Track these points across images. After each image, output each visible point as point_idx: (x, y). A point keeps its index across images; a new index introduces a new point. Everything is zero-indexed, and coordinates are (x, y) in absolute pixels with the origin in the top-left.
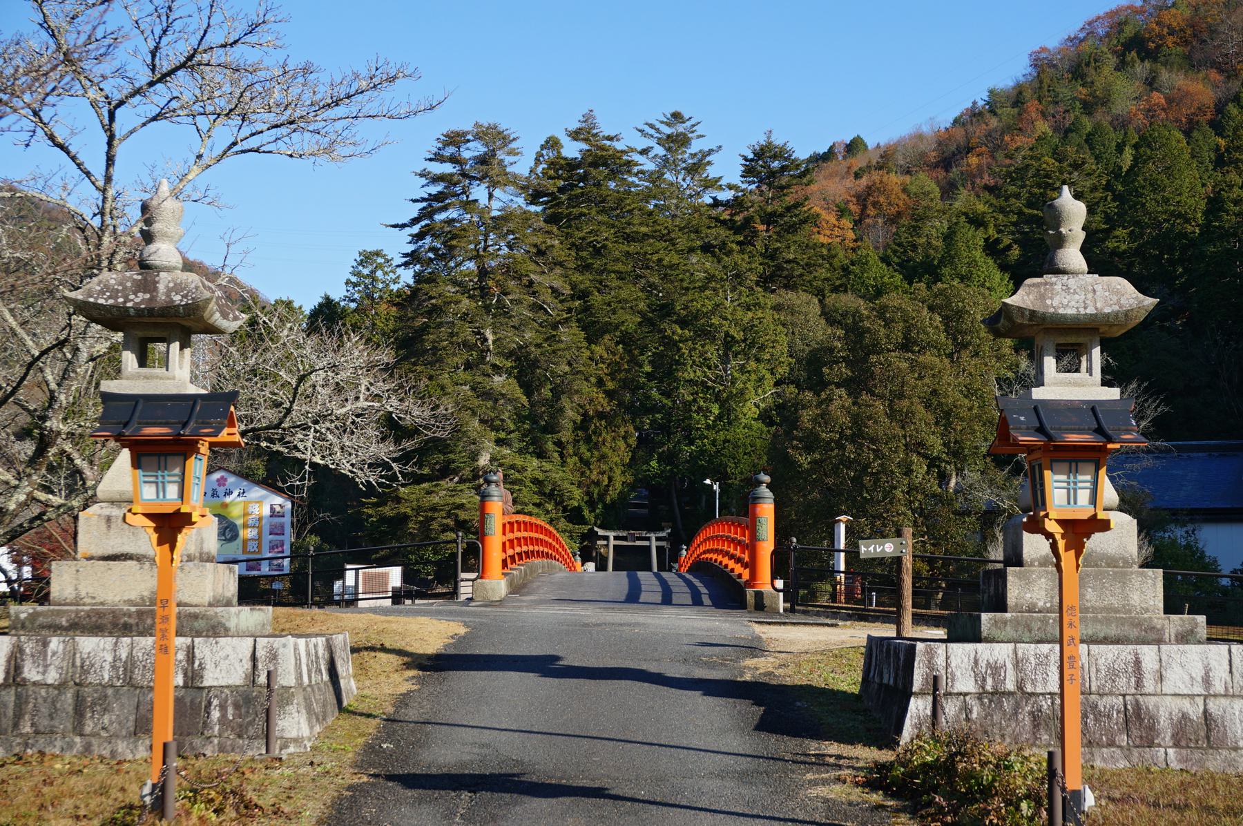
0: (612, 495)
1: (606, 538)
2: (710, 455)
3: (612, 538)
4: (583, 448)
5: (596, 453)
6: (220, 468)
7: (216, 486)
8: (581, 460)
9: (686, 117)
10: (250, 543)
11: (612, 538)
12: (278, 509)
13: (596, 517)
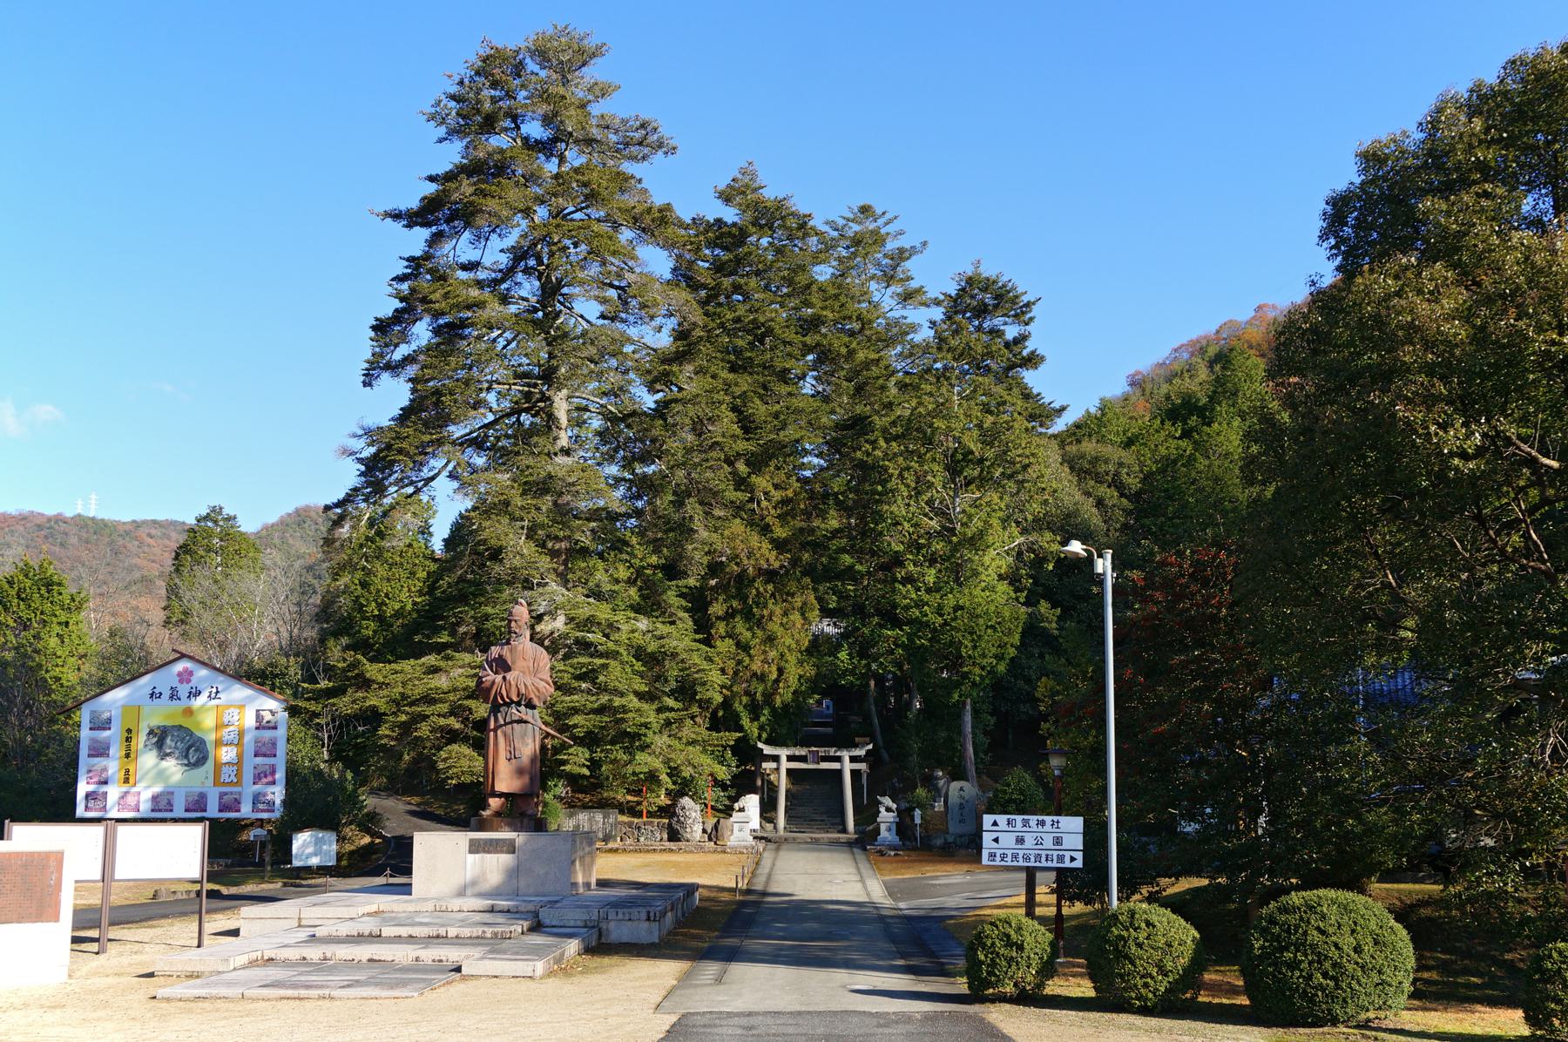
0: (784, 696)
1: (776, 759)
2: (935, 630)
3: (784, 759)
4: (740, 626)
5: (759, 633)
6: (183, 656)
7: (175, 683)
8: (738, 645)
9: (879, 211)
10: (225, 769)
11: (784, 759)
12: (267, 716)
13: (761, 728)
